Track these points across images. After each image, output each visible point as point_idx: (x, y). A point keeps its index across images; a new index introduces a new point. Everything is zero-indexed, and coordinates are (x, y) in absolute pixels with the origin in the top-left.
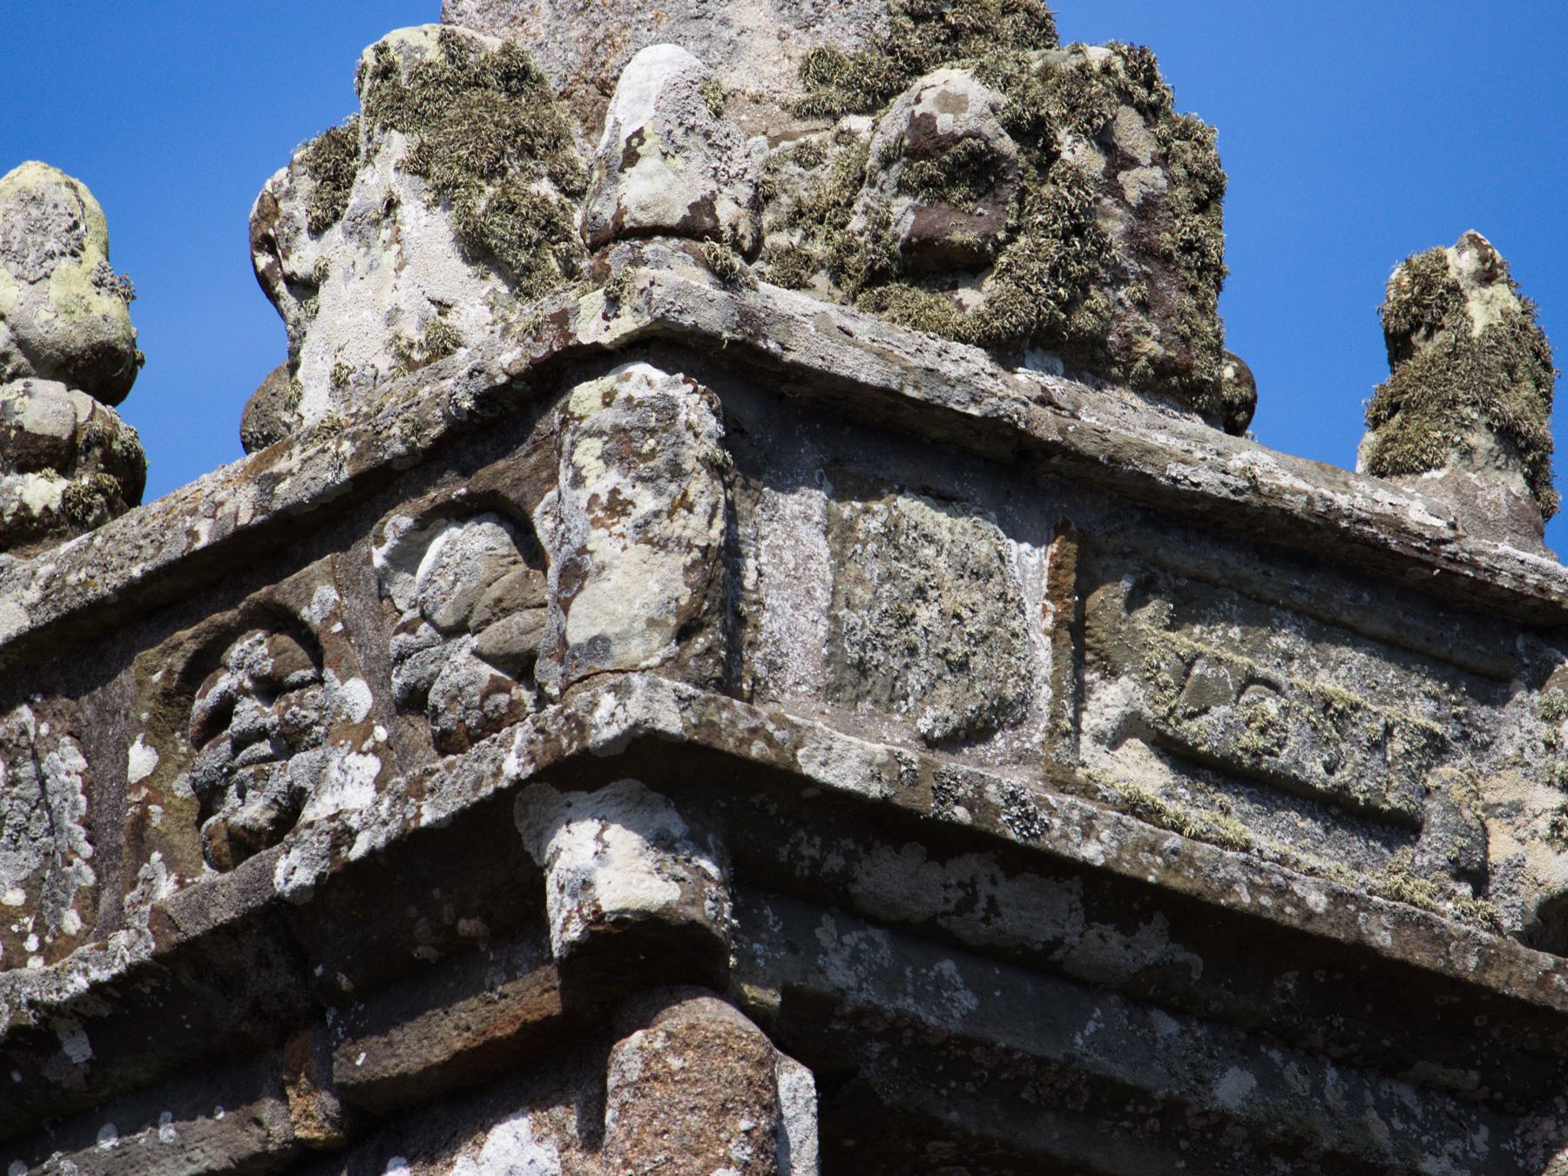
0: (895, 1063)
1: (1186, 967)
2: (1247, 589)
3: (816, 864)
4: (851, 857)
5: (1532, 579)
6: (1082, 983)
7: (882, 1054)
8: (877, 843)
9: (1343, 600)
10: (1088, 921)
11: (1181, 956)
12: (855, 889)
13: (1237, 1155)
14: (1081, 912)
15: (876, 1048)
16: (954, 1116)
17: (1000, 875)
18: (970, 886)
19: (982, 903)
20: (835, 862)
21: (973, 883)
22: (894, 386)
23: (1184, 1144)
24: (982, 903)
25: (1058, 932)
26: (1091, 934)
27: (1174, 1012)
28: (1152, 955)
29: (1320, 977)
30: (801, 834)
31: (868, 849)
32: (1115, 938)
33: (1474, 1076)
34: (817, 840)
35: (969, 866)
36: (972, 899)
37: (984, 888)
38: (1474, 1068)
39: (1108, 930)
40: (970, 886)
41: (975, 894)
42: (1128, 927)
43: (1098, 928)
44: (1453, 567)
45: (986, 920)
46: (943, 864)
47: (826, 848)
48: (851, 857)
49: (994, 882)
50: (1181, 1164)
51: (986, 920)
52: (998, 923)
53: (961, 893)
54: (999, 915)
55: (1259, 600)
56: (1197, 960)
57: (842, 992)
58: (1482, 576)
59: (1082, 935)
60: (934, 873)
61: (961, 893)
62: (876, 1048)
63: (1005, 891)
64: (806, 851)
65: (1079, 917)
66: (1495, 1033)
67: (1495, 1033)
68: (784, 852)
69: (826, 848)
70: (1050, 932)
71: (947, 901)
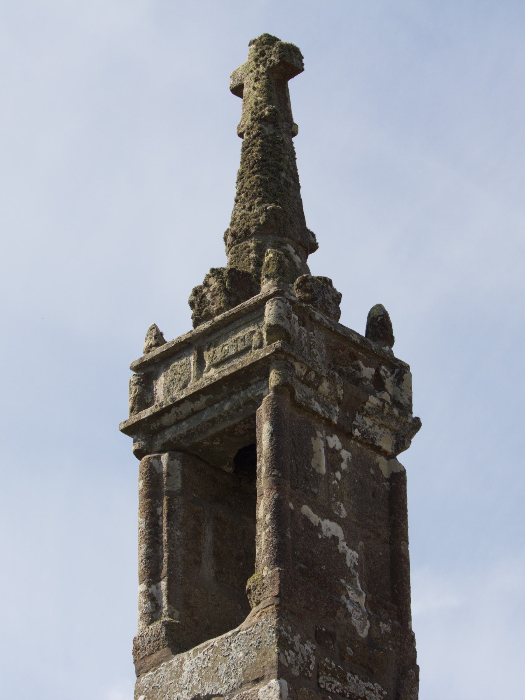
0: (185, 440)
1: (210, 397)
2: (224, 334)
3: (157, 426)
4: (160, 422)
5: (255, 300)
6: (203, 410)
7: (183, 441)
8: (161, 417)
9: (237, 324)
10: (193, 403)
11: (208, 397)
12: (164, 425)
13: (235, 414)
14: (191, 403)
15: (181, 441)
16: (197, 440)
17: (178, 408)
18: (176, 412)
19: (179, 413)
20: (158, 424)
21: (176, 412)
22: (162, 351)
23: (227, 418)
24: (179, 413)
25: (191, 408)
26: (195, 405)
27: (216, 403)
28: (205, 400)
29: (227, 384)
30: (152, 424)
31: (161, 419)
32: (198, 402)
33: (258, 377)
34: (154, 424)
35: (173, 410)
36: (177, 413)
37: (178, 411)
38: (256, 376)
39: (197, 402)
40: (176, 412)
41: (177, 413)
42: (198, 399)
43: (195, 403)
44: (244, 308)
45: (181, 414)
46: (171, 413)
47: (156, 423)
48: (160, 422)
49: (178, 409)
50: (229, 421)
51: (181, 414)
52: (183, 413)
53: (176, 414)
54: (182, 412)
55: (226, 333)
56: (211, 396)
57: (169, 439)
58: (249, 305)
59: (194, 406)
60: (170, 415)
61: (176, 414)
62: (181, 441)
63: (180, 409)
64: (154, 426)
65: (192, 404)
66: (255, 370)
67: (255, 370)
68: (152, 429)
69: (156, 423)
70: (190, 409)
71: (175, 416)
